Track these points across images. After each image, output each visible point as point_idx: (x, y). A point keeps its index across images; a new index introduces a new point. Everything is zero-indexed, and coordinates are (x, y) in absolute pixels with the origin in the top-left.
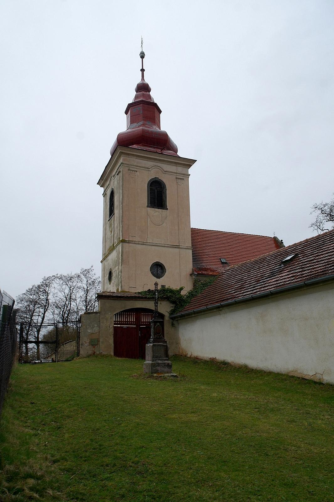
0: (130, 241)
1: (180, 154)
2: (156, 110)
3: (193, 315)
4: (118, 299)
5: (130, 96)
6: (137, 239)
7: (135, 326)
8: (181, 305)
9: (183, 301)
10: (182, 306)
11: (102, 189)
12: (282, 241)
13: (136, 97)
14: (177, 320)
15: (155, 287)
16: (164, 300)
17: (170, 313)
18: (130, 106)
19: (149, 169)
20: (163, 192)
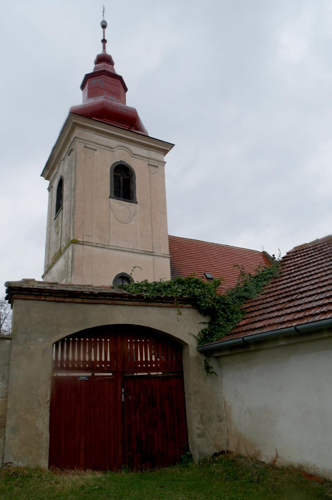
0: (85, 242)
4: (66, 300)
5: (90, 68)
6: (94, 240)
7: (111, 374)
11: (48, 182)
12: (274, 255)
13: (95, 69)
18: (88, 77)
19: (113, 148)
20: (131, 180)
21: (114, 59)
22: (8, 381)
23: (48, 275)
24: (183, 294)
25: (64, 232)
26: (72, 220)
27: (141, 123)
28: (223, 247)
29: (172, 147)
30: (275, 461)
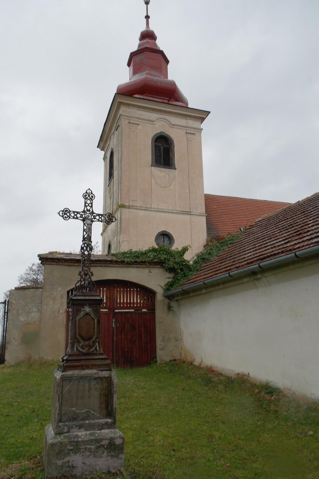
0: (131, 206)
1: (189, 106)
2: (162, 59)
3: (204, 291)
4: (75, 264)
5: (134, 45)
6: (139, 204)
7: (133, 310)
8: (184, 274)
9: (187, 267)
10: (185, 276)
11: (103, 153)
14: (177, 300)
15: (86, 203)
16: (155, 266)
17: (165, 288)
18: (133, 55)
19: (154, 121)
21: (157, 34)
22: (41, 312)
23: (105, 233)
24: (154, 259)
25: (115, 197)
26: (120, 188)
27: (180, 93)
28: (261, 202)
29: (209, 113)
30: (200, 364)
